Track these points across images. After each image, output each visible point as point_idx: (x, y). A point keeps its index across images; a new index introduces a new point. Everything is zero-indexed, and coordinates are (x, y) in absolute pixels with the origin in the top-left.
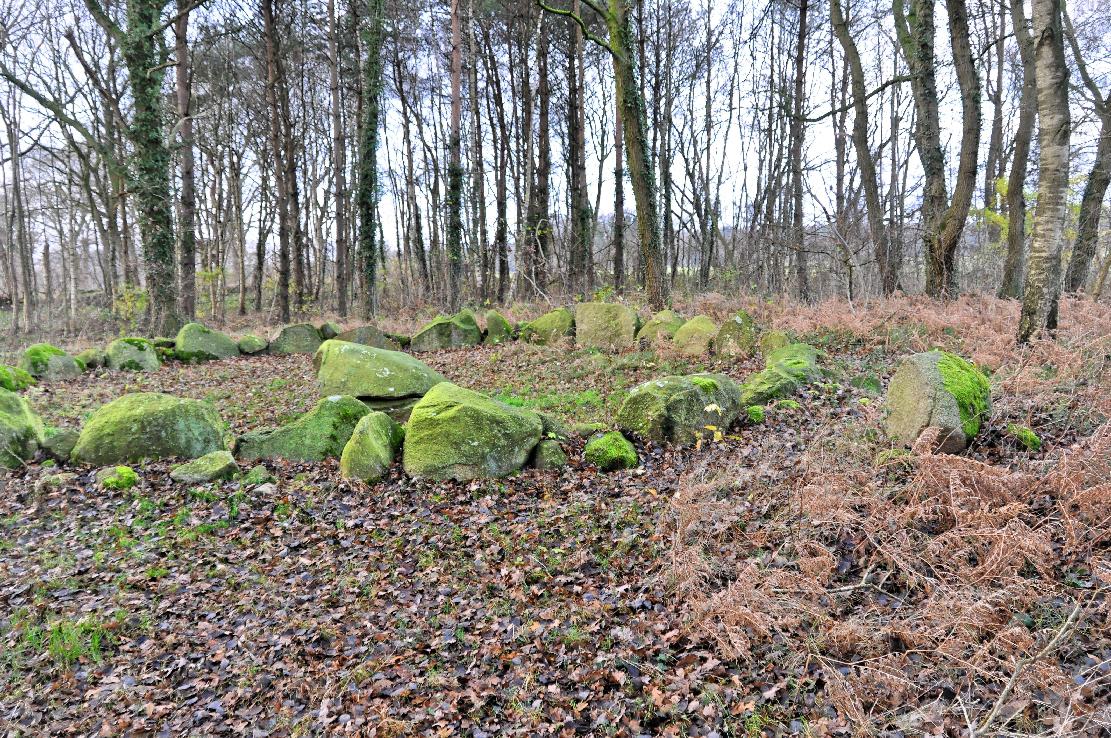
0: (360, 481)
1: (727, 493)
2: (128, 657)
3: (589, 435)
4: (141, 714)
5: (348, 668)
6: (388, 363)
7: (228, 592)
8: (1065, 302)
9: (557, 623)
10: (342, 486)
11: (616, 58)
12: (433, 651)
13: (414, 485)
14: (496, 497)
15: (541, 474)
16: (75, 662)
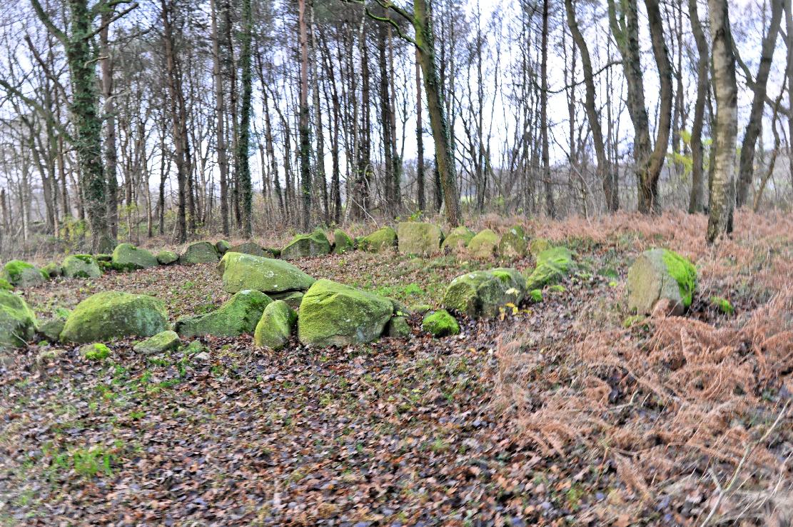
0: (267, 347)
1: (525, 349)
2: (131, 471)
3: (424, 313)
4: (149, 508)
5: (287, 472)
6: (271, 267)
7: (190, 427)
8: (737, 215)
9: (424, 438)
10: (256, 352)
12: (343, 459)
13: (307, 350)
14: (365, 357)
15: (394, 340)
16: (95, 477)
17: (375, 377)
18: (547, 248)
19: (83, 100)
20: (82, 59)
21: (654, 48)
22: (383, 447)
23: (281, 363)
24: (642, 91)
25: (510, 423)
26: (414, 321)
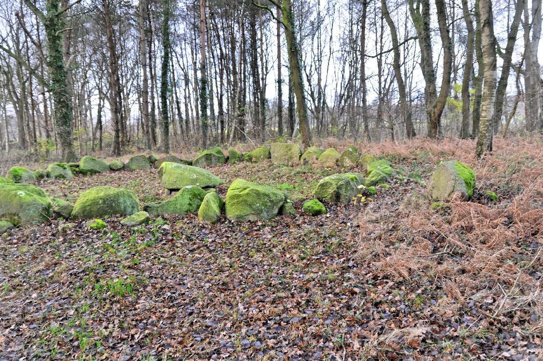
0: (207, 222)
6: (195, 172)
9: (320, 273)
10: (201, 225)
11: (286, 28)
12: (274, 286)
13: (233, 223)
17: (279, 240)
19: (55, 57)
20: (54, 29)
21: (440, 28)
22: (296, 279)
23: (217, 231)
24: (432, 57)
25: (371, 264)
26: (298, 205)
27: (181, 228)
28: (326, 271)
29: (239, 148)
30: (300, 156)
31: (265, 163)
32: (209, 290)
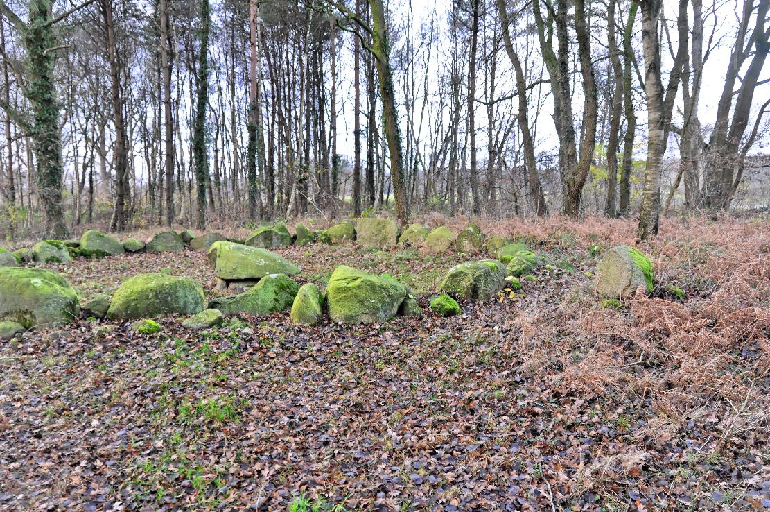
0: (305, 324)
12: (425, 406)
13: (340, 326)
18: (504, 245)
19: (41, 87)
20: (41, 47)
25: (546, 378)
26: (423, 302)
27: (270, 332)
28: (489, 388)
29: (307, 223)
30: (398, 237)
31: (349, 246)
32: (340, 413)
